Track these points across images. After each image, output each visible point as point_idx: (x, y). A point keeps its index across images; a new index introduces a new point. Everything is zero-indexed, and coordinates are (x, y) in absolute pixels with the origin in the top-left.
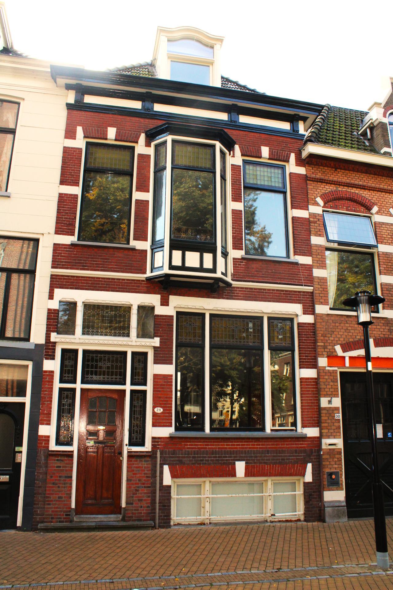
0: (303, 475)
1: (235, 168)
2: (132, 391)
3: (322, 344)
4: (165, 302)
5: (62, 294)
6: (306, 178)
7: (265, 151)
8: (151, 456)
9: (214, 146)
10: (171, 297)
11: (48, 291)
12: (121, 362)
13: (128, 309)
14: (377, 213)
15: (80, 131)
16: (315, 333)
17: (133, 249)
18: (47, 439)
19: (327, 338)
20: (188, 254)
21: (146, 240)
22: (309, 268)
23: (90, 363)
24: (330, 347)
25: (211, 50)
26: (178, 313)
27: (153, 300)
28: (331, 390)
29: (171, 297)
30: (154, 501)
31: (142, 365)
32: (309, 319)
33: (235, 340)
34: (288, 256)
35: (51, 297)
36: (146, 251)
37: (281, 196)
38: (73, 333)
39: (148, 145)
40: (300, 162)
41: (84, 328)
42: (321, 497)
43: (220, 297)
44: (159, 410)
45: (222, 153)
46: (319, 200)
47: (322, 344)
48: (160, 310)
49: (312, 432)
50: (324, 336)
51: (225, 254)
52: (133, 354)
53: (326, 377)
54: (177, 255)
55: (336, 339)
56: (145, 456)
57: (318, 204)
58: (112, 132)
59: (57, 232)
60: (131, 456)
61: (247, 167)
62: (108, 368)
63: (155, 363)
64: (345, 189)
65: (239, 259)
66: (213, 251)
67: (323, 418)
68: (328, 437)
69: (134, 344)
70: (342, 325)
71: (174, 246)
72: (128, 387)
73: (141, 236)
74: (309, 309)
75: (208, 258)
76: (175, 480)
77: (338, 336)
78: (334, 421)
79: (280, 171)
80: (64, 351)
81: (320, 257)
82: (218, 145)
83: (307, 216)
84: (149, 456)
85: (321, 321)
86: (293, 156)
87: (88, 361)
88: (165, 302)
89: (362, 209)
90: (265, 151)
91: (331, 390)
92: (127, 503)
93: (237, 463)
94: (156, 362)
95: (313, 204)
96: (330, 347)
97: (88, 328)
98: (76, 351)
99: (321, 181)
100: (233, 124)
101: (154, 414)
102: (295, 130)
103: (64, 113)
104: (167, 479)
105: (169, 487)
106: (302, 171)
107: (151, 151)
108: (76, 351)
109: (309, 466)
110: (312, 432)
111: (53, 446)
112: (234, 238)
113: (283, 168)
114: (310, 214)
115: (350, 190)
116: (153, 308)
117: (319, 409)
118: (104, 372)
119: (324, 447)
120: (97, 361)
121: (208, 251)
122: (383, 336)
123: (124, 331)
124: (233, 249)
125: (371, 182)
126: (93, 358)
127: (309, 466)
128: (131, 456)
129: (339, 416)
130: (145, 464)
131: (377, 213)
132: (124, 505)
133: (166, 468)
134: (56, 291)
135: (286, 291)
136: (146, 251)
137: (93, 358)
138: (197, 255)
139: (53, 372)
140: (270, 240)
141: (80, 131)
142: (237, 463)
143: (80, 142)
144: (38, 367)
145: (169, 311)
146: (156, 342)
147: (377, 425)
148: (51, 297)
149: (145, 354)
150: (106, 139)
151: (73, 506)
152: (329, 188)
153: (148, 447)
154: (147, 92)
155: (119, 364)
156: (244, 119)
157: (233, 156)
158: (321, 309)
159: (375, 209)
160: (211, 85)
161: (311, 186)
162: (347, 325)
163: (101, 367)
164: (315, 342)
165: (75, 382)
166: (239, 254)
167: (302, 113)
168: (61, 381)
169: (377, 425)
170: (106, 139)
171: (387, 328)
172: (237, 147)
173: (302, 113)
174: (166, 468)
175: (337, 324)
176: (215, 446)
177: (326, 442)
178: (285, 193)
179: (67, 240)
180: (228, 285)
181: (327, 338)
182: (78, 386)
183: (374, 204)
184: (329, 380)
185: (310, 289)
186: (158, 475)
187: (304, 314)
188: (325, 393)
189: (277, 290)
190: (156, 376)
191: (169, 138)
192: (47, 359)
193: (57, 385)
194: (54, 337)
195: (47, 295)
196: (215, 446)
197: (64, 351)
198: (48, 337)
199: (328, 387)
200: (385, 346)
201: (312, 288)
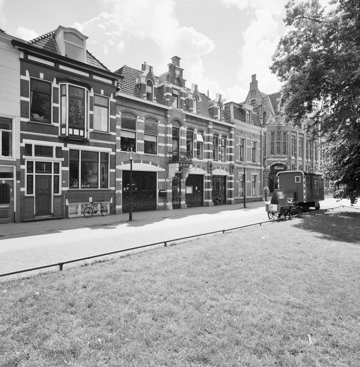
0: (110, 201)
1: (91, 97)
2: (54, 176)
4: (66, 146)
5: (26, 141)
6: (116, 104)
7: (102, 92)
8: (61, 197)
9: (84, 89)
10: (68, 144)
11: (20, 139)
13: (52, 148)
14: (139, 119)
15: (27, 72)
16: (115, 158)
17: (53, 126)
18: (24, 192)
20: (75, 130)
21: (58, 123)
22: (115, 137)
23: (38, 166)
25: (82, 41)
26: (70, 149)
27: (61, 145)
29: (68, 144)
30: (63, 211)
31: (57, 167)
32: (114, 153)
34: (108, 132)
35: (21, 142)
36: (58, 127)
37: (107, 109)
38: (31, 155)
39: (57, 83)
40: (115, 97)
41: (35, 153)
42: (115, 207)
43: (85, 145)
44: (64, 182)
45: (87, 92)
46: (120, 113)
48: (64, 149)
49: (113, 188)
51: (87, 131)
52: (54, 163)
54: (71, 130)
56: (60, 197)
57: (119, 114)
58: (42, 76)
59: (21, 116)
60: (55, 197)
61: (95, 97)
63: (62, 166)
64: (129, 109)
66: (83, 129)
69: (55, 160)
71: (69, 127)
72: (53, 174)
73: (56, 121)
74: (114, 150)
75: (82, 132)
76: (70, 204)
79: (107, 100)
80: (28, 162)
82: (86, 89)
84: (61, 197)
86: (112, 95)
88: (66, 146)
89: (134, 116)
90: (102, 92)
92: (54, 211)
94: (63, 166)
97: (37, 154)
98: (32, 162)
99: (121, 106)
100: (90, 79)
101: (62, 183)
102: (113, 84)
103: (18, 63)
104: (67, 203)
105: (68, 206)
106: (115, 101)
107: (58, 86)
108: (32, 162)
109: (112, 198)
110: (113, 188)
111: (26, 195)
112: (90, 124)
113: (108, 99)
114: (116, 117)
115: (130, 109)
116: (61, 148)
119: (116, 193)
121: (82, 129)
123: (51, 155)
125: (138, 107)
126: (39, 164)
127: (112, 198)
128: (55, 197)
129: (121, 184)
130: (59, 200)
131: (139, 119)
132: (52, 212)
133: (67, 200)
134: (24, 140)
136: (58, 127)
137: (39, 164)
138: (78, 131)
139: (24, 169)
141: (27, 72)
143: (27, 78)
144: (18, 167)
145: (67, 149)
146: (63, 159)
147: (23, 139)
148: (21, 142)
149: (59, 163)
150: (39, 78)
151: (35, 214)
152: (124, 108)
153: (60, 194)
154: (56, 60)
155: (49, 167)
156: (95, 77)
159: (138, 117)
160: (82, 62)
161: (118, 107)
164: (115, 161)
165: (51, 173)
166: (91, 130)
167: (117, 78)
168: (27, 173)
169: (23, 139)
170: (39, 78)
172: (92, 89)
173: (117, 78)
174: (67, 200)
176: (83, 193)
177: (117, 191)
178: (108, 108)
179: (27, 120)
182: (34, 174)
185: (114, 143)
186: (63, 202)
190: (63, 171)
191: (67, 84)
192: (21, 165)
193: (26, 174)
194: (24, 157)
195: (19, 141)
196: (83, 193)
197: (28, 162)
198: (21, 157)
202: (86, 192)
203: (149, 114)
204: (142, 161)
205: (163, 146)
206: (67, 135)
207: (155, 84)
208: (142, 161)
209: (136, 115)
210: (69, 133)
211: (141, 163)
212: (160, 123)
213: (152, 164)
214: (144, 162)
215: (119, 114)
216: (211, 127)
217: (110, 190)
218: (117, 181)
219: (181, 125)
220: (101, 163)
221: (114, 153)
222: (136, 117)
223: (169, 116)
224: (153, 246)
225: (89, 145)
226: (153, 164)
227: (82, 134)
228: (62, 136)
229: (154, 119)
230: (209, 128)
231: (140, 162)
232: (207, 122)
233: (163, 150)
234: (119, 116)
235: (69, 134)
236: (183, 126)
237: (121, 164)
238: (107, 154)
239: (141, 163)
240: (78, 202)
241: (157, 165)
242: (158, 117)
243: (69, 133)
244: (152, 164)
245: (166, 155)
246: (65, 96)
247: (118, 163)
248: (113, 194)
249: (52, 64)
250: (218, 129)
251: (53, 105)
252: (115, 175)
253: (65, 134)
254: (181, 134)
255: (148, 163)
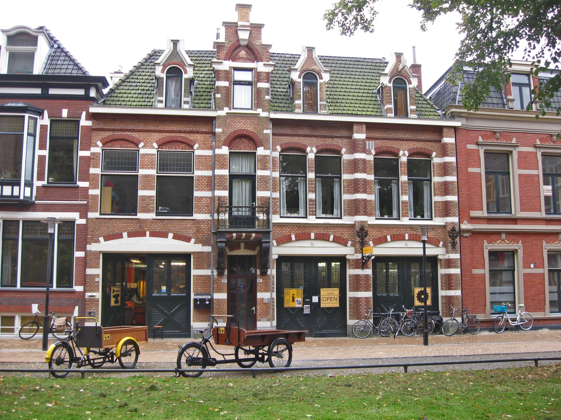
3: (91, 237)
12: (71, 227)
19: (94, 233)
22: (86, 189)
24: (96, 238)
28: (94, 264)
32: (83, 221)
33: (37, 235)
46: (99, 143)
47: (91, 237)
50: (92, 231)
53: (92, 257)
55: (100, 233)
57: (97, 146)
58: (65, 113)
62: (69, 230)
65: (40, 187)
67: (87, 281)
68: (90, 291)
70: (105, 224)
74: (83, 215)
75: (16, 189)
77: (102, 231)
78: (94, 282)
81: (95, 181)
83: (89, 155)
85: (91, 222)
87: (25, 226)
91: (94, 264)
93: (33, 305)
95: (94, 146)
96: (96, 238)
106: (89, 123)
109: (77, 308)
110: (79, 288)
114: (91, 153)
117: (85, 276)
118: (66, 233)
119: (86, 297)
120: (34, 226)
122: (134, 230)
124: (37, 180)
125: (141, 127)
127: (77, 308)
135: (70, 205)
138: (10, 188)
140: (337, 29)
142: (33, 305)
152: (106, 134)
157: (43, 118)
158: (91, 215)
162: (109, 224)
163: (64, 230)
166: (41, 183)
171: (138, 225)
172: (46, 112)
175: (102, 224)
180: (33, 204)
181: (94, 233)
183: (140, 141)
184: (93, 258)
187: (80, 218)
188: (90, 266)
189: (64, 205)
199: (92, 262)
200: (135, 237)
201: (86, 202)
202: (27, 295)
203: (168, 135)
204: (148, 233)
205: (208, 197)
206: (22, 198)
207: (186, 73)
208: (148, 233)
209: (136, 141)
210: (25, 195)
211: (145, 236)
212: (436, 157)
213: (174, 238)
214: (153, 234)
215: (97, 146)
216: (359, 136)
217: (74, 292)
218: (89, 275)
219: (256, 146)
220: (498, 212)
221: (83, 221)
222: (137, 145)
223: (218, 130)
224: (322, 370)
225: (34, 210)
226: (177, 237)
227: (16, 193)
228: (25, 199)
229: (182, 142)
230: (356, 141)
231: (145, 235)
232: (439, 130)
233: (207, 206)
234: (97, 149)
235: (24, 196)
236: (261, 145)
237: (98, 241)
238: (71, 223)
239: (145, 236)
240: (13, 312)
241: (188, 240)
242: (192, 137)
243: (25, 195)
244: (174, 238)
245: (212, 216)
246: (29, 134)
247: (92, 238)
248: (80, 299)
249: (38, 91)
250: (386, 139)
251: (46, 153)
252: (85, 263)
253: (19, 197)
254: (433, 169)
255: (165, 235)
